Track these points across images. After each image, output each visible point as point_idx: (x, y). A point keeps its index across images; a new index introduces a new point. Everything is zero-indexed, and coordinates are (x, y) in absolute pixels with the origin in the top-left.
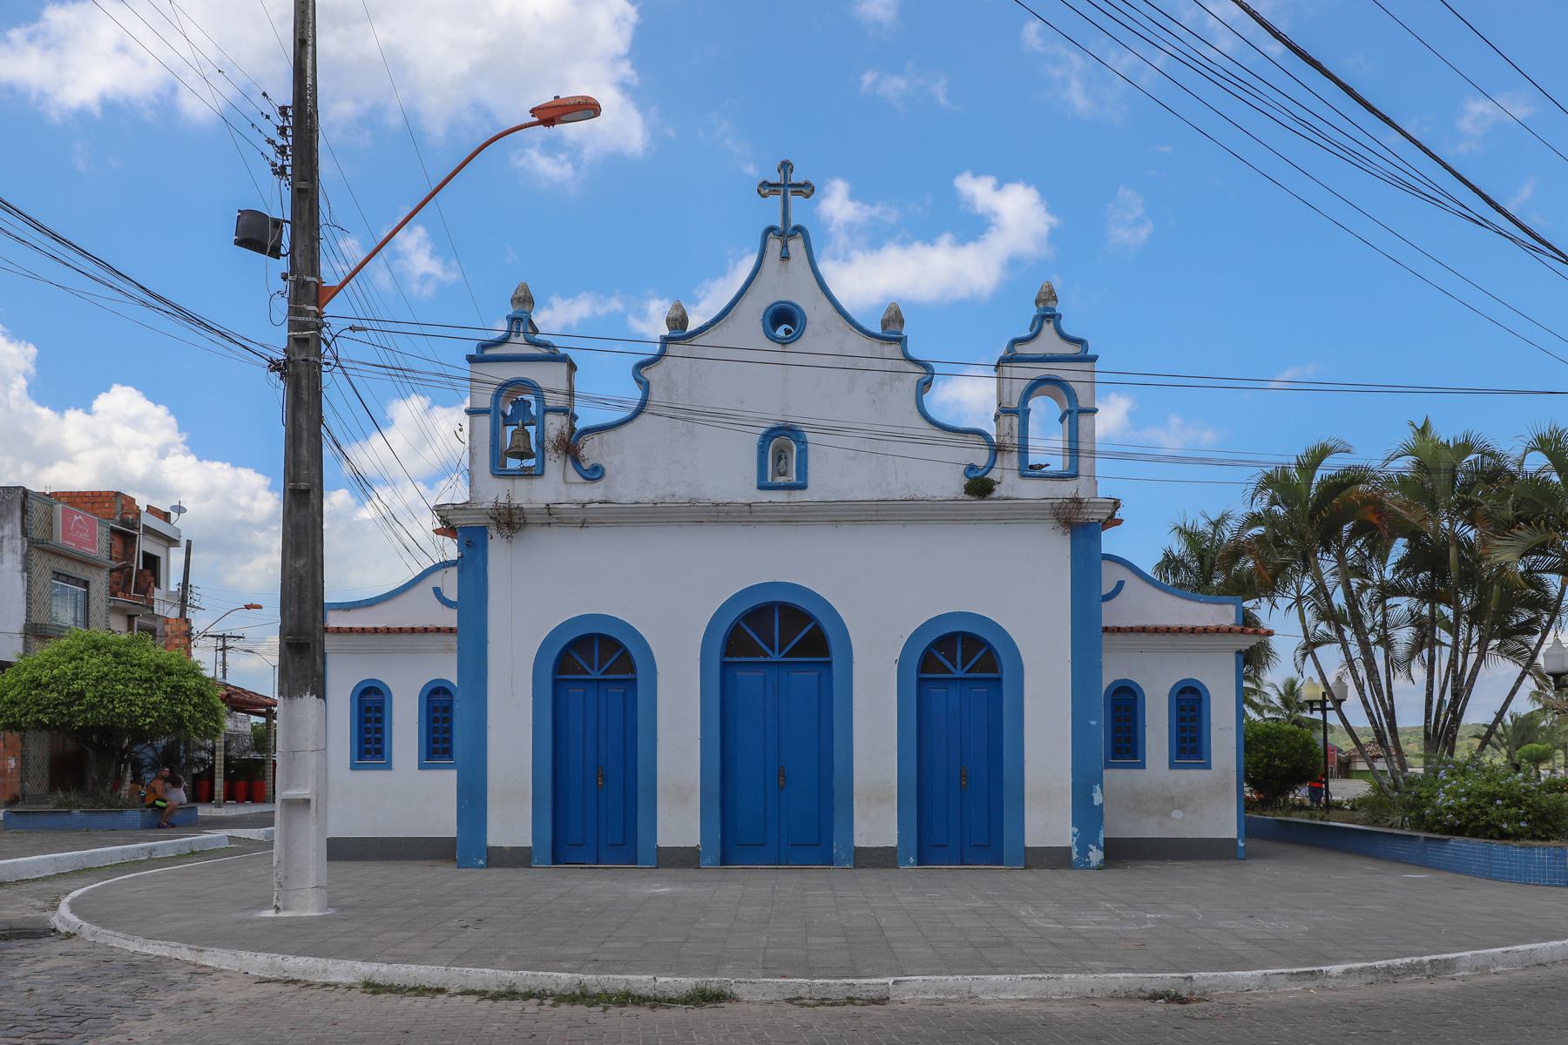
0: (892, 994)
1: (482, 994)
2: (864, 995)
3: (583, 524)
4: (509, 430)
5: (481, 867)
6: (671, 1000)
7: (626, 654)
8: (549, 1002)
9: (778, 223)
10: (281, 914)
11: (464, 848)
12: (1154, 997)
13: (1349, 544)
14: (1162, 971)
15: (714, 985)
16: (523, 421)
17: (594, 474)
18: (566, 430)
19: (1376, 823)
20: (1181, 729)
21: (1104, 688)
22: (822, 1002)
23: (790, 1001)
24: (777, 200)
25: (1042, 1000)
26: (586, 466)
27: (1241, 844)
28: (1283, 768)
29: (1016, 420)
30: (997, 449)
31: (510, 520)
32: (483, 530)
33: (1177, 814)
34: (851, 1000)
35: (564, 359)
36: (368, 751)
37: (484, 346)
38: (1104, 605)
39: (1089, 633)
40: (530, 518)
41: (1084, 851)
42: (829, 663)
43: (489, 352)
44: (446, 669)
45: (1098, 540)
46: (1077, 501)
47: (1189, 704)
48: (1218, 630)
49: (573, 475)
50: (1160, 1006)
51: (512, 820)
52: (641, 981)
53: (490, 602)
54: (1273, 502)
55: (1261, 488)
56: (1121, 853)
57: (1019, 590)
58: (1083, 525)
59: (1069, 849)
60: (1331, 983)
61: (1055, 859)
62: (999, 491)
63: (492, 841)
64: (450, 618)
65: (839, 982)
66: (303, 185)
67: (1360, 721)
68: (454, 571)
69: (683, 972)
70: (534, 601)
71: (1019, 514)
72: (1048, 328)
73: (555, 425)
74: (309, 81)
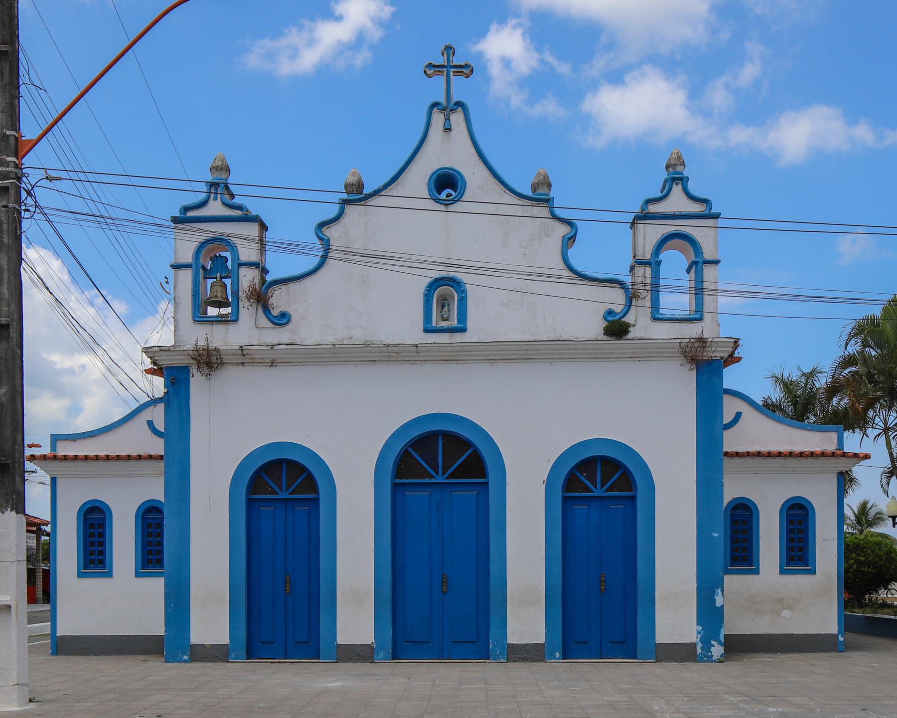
3: (273, 364)
5: (185, 661)
17: (282, 320)
26: (275, 312)
30: (632, 297)
31: (209, 360)
33: (786, 613)
35: (256, 219)
37: (187, 209)
40: (226, 359)
41: (707, 646)
43: (190, 214)
46: (702, 341)
49: (263, 321)
59: (835, 637)
61: (681, 653)
62: (633, 333)
63: (194, 640)
71: (651, 352)
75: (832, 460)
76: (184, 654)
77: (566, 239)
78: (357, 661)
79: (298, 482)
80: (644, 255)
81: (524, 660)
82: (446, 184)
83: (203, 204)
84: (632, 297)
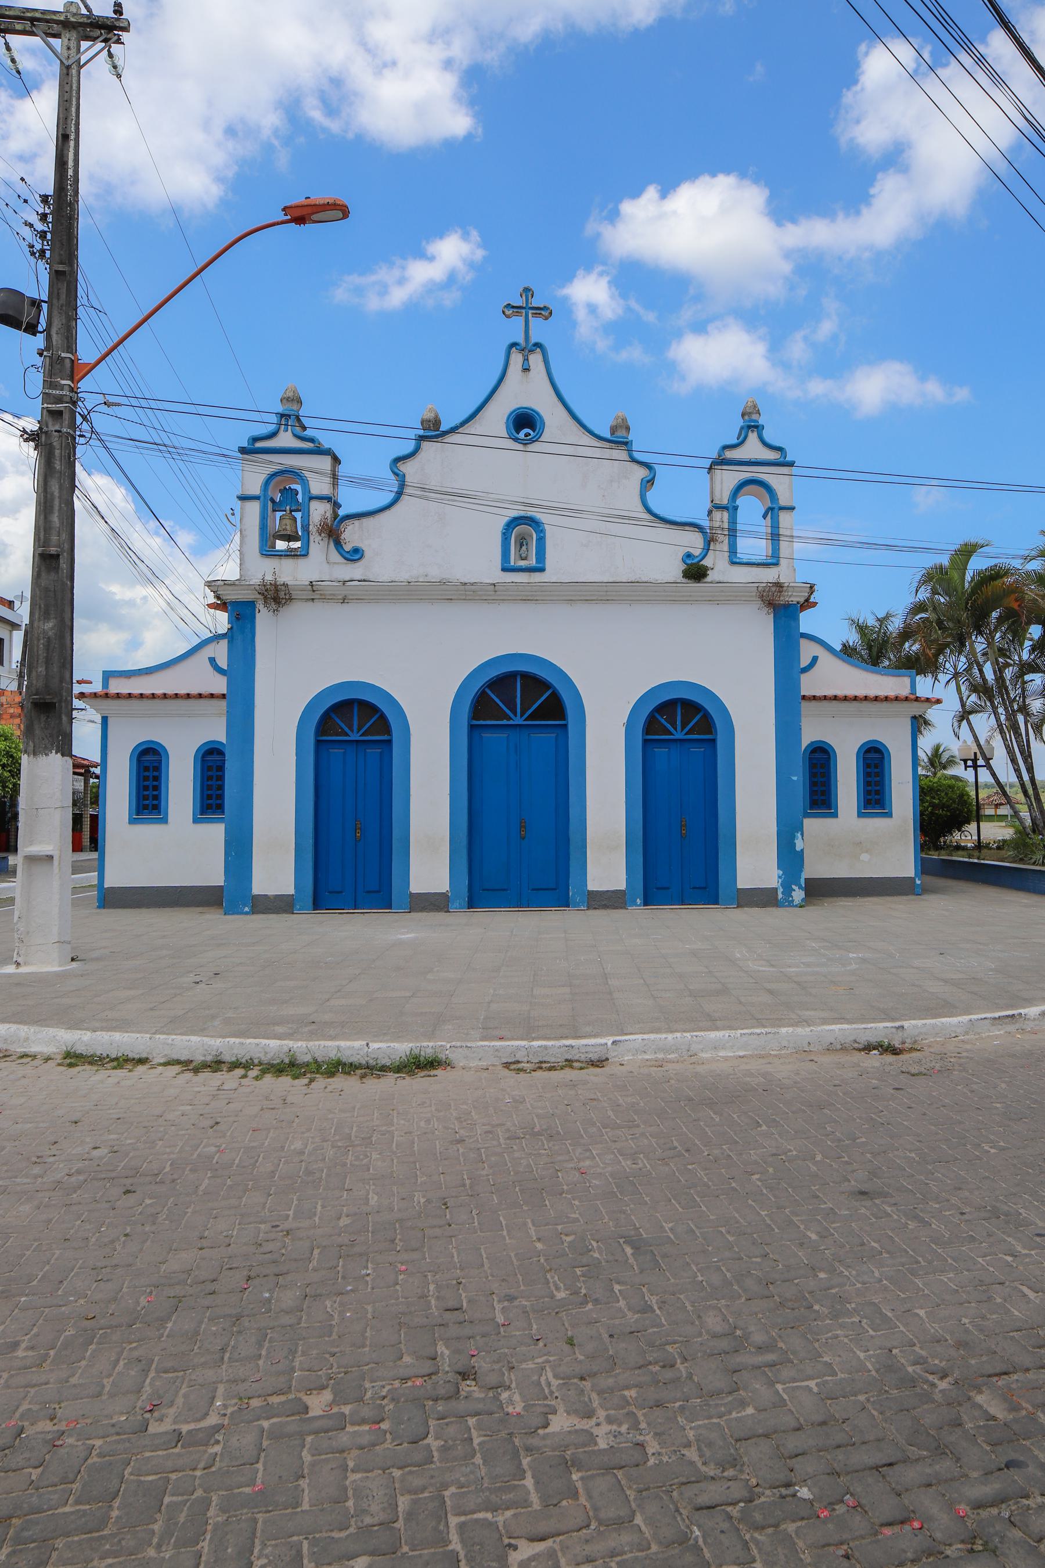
0: (611, 1055)
1: (186, 1065)
2: (583, 1057)
3: (344, 600)
4: (279, 514)
5: (247, 913)
6: (384, 1069)
7: (383, 717)
8: (254, 1072)
9: (521, 340)
10: (22, 970)
11: (230, 895)
12: (868, 1048)
13: (996, 630)
14: (874, 1020)
15: (429, 1051)
16: (293, 504)
17: (355, 555)
18: (329, 515)
19: (1021, 860)
20: (867, 783)
21: (803, 748)
22: (540, 1066)
23: (507, 1065)
24: (519, 321)
25: (762, 1057)
26: (348, 548)
27: (918, 882)
28: (943, 812)
29: (726, 515)
30: (710, 541)
31: (276, 596)
32: (252, 604)
33: (865, 857)
34: (569, 1063)
35: (328, 452)
36: (146, 807)
37: (256, 439)
38: (802, 676)
39: (790, 700)
42: (566, 726)
43: (259, 445)
44: (217, 731)
45: (797, 619)
46: (778, 585)
47: (874, 760)
48: (897, 699)
50: (875, 1059)
51: (276, 870)
52: (352, 1048)
53: (257, 670)
54: (934, 592)
55: (923, 582)
56: (820, 890)
57: (732, 666)
58: (784, 609)
60: (1029, 1026)
62: (712, 576)
63: (257, 889)
64: (220, 685)
65: (557, 1043)
66: (61, 268)
67: (1006, 774)
68: (224, 643)
69: (397, 1038)
70: (296, 671)
71: (729, 595)
72: (753, 437)
73: (319, 511)
74: (70, 172)
75: (906, 704)
76: (245, 905)
77: (644, 482)
78: (431, 910)
79: (369, 724)
80: (721, 499)
81: (605, 907)
82: (525, 423)
83: (273, 435)
84: (710, 541)
